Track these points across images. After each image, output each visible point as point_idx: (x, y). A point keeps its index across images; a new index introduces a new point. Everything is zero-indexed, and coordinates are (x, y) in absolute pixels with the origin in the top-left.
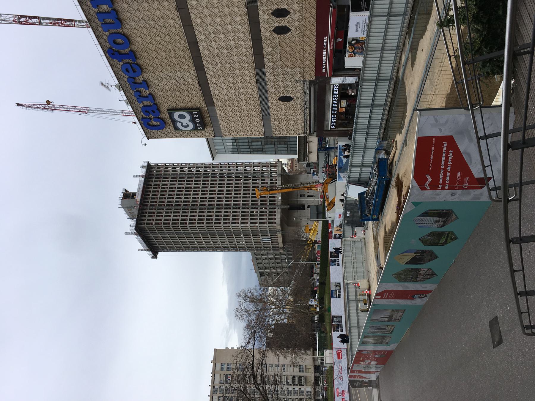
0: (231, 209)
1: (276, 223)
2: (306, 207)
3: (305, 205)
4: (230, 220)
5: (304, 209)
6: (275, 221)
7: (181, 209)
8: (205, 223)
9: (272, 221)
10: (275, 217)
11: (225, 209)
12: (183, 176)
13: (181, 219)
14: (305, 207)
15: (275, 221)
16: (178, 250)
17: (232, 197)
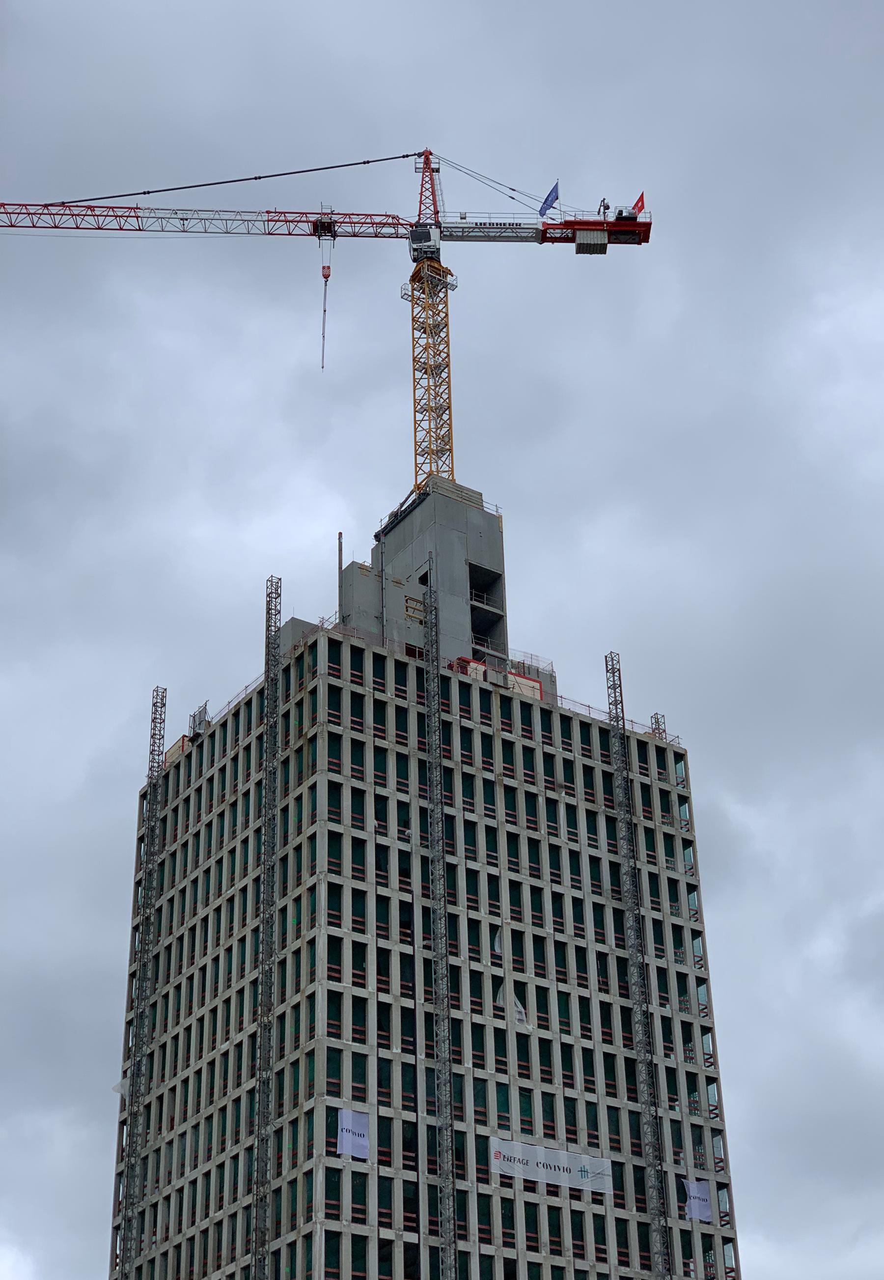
0: (433, 1233)
4: (355, 1220)
7: (434, 1180)
8: (334, 1043)
11: (432, 1188)
12: (643, 1088)
16: (141, 1016)
17: (512, 1245)
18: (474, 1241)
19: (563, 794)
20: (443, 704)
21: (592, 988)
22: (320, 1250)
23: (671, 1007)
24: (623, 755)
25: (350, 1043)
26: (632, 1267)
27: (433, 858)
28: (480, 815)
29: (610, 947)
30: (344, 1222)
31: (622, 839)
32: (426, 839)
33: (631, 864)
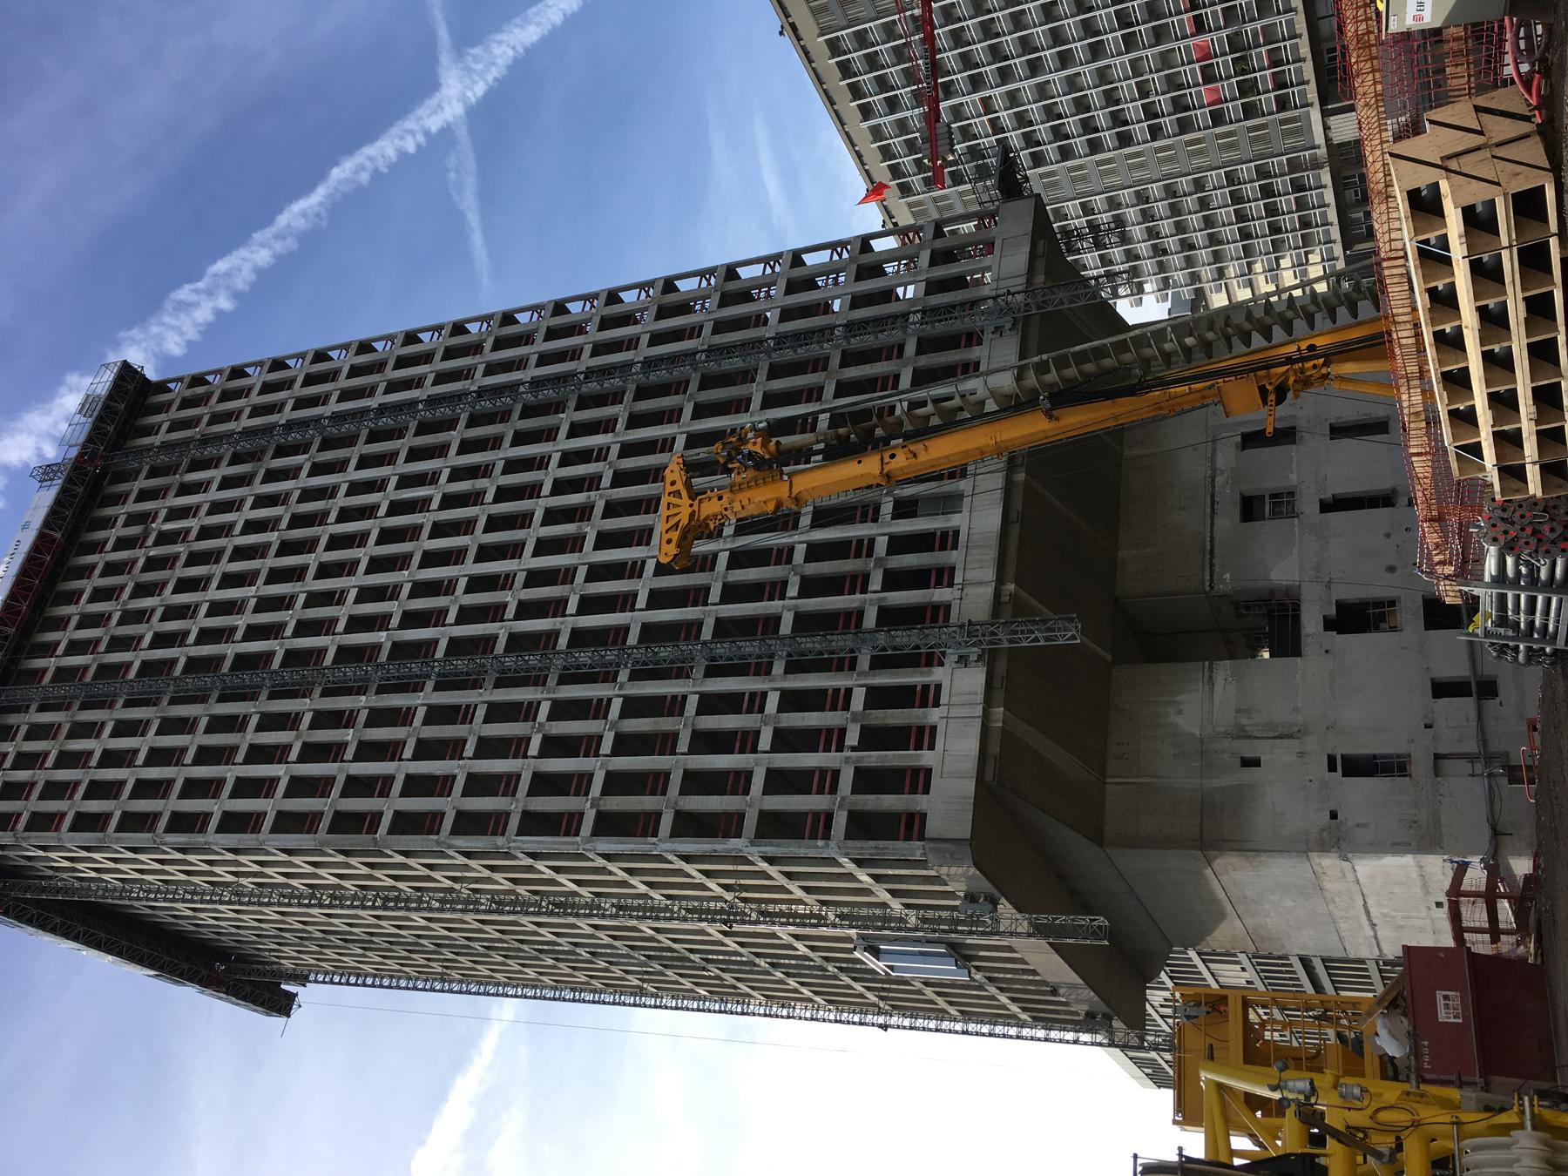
1: (933, 827)
2: (1311, 622)
3: (1297, 607)
5: (1288, 644)
6: (920, 802)
9: (889, 802)
10: (926, 758)
13: (688, 774)
14: (1297, 618)
15: (920, 802)
18: (562, 623)
19: (154, 525)
20: (934, 620)
21: (550, 449)
22: (542, 842)
23: (769, 310)
24: (721, 354)
25: (330, 800)
26: (618, 415)
27: (707, 660)
28: (149, 629)
29: (307, 460)
30: (513, 806)
31: (494, 405)
32: (476, 681)
33: (703, 357)
